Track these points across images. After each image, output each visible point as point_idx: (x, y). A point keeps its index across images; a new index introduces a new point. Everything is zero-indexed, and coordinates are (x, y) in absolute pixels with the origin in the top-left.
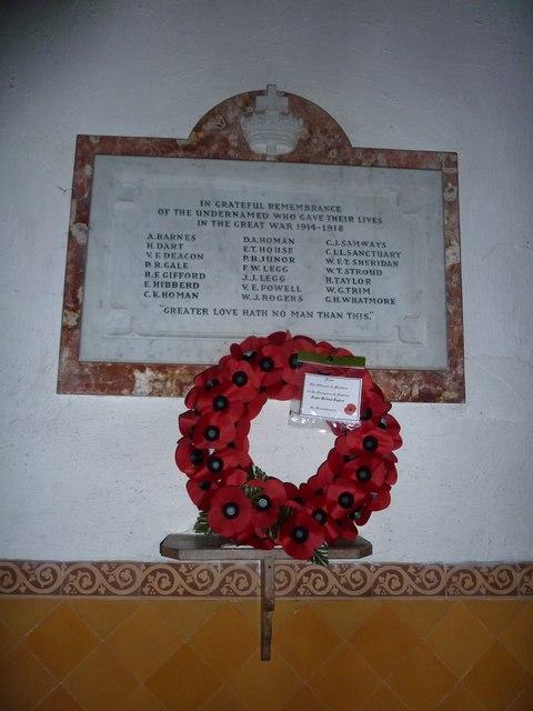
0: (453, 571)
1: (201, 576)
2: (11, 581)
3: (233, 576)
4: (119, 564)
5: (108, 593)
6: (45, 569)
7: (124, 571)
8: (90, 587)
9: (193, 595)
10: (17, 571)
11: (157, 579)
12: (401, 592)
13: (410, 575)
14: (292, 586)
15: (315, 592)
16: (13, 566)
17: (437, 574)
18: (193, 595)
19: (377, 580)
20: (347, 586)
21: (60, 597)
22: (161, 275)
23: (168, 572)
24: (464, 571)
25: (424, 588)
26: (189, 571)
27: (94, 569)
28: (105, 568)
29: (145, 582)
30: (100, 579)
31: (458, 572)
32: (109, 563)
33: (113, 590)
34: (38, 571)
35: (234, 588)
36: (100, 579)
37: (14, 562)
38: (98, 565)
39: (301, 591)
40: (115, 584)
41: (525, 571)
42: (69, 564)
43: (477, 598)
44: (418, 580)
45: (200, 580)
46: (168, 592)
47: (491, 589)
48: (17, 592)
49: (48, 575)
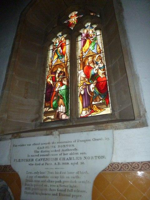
0: (122, 164)
1: (136, 165)
2: (128, 168)
3: (144, 165)
4: (134, 162)
5: (112, 170)
6: (136, 164)
7: (136, 164)
8: (108, 169)
9: (114, 171)
10: (128, 164)
11: (145, 166)
12: (109, 170)
13: (130, 165)
14: (120, 168)
15: (146, 169)
16: (127, 164)
17: (118, 165)
18: (114, 171)
19: (142, 166)
20: (134, 168)
21: (121, 171)
22: (34, 160)
23: (127, 165)
24: (125, 164)
25: (115, 169)
26: (132, 164)
27: (128, 164)
28: (131, 164)
29: (3, 169)
30: (130, 166)
31: (124, 164)
32: (131, 163)
33: (134, 169)
34: (114, 165)
35: (145, 168)
36: (130, 166)
37: (127, 163)
38: (128, 163)
39: (122, 169)
40: (114, 168)
41: (142, 164)
42: (142, 162)
43: (110, 172)
44: (113, 167)
45: (116, 167)
46: (128, 170)
47: (113, 169)
48: (7, 171)
49: (116, 166)
